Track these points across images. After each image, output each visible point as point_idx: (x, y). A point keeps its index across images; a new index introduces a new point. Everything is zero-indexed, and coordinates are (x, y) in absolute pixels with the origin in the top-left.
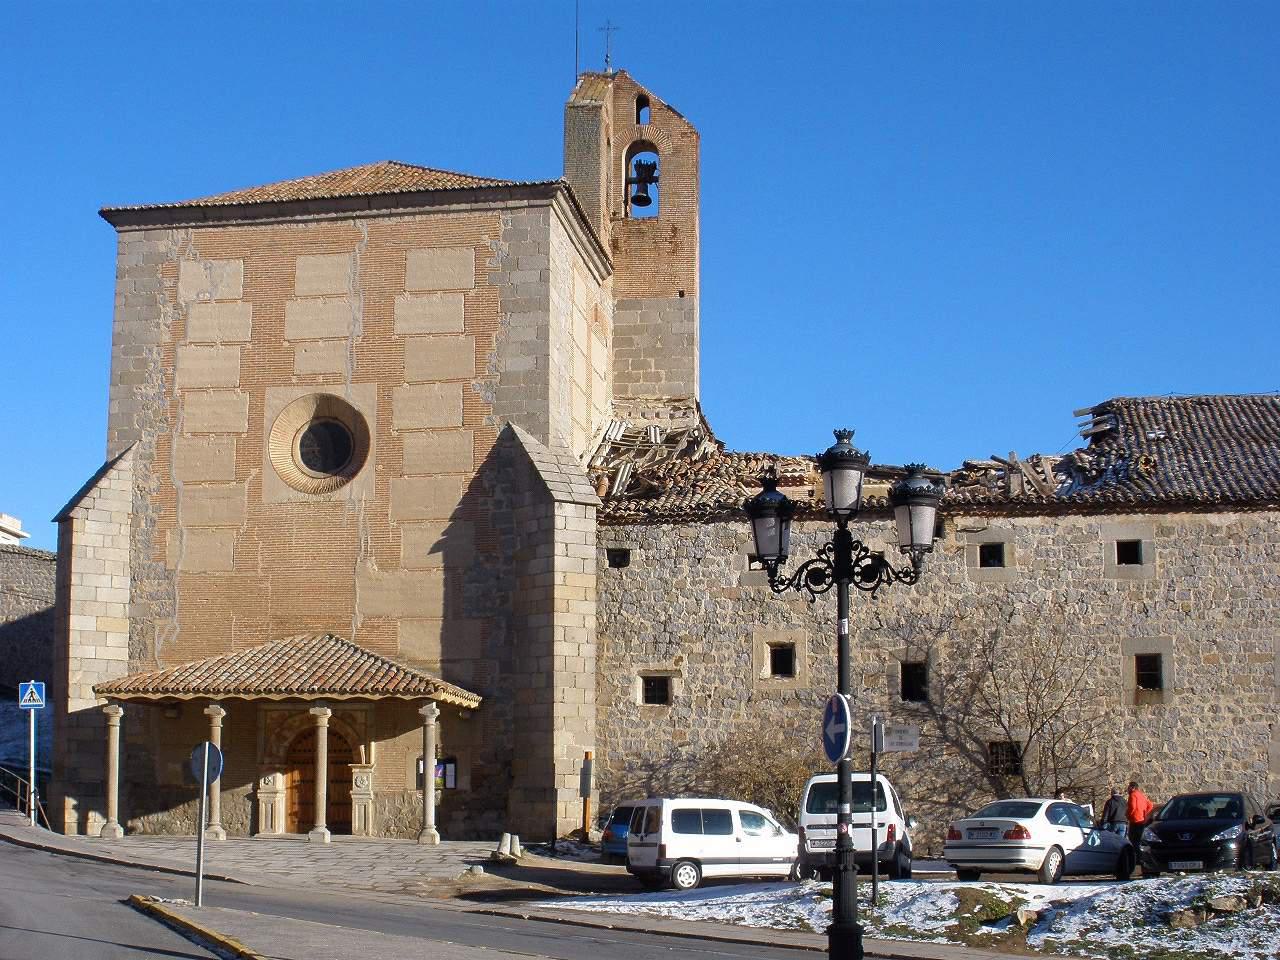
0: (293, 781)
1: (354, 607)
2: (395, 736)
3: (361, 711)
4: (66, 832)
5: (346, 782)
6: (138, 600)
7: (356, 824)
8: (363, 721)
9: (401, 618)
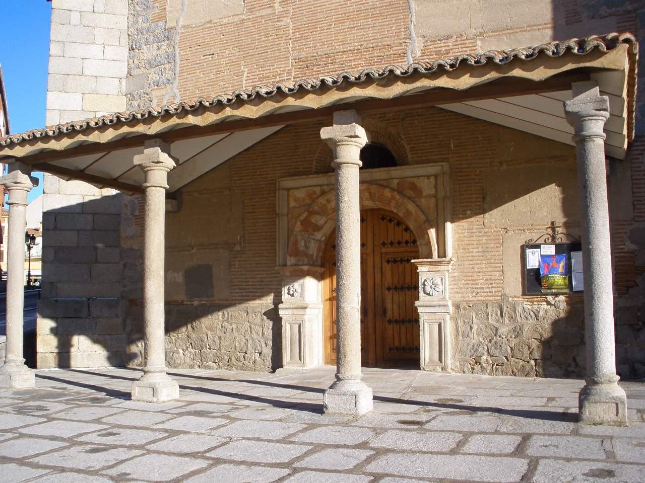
1: (409, 29)
2: (484, 211)
3: (428, 177)
4: (38, 364)
5: (409, 288)
6: (135, 72)
7: (427, 352)
8: (433, 192)
9: (481, 34)
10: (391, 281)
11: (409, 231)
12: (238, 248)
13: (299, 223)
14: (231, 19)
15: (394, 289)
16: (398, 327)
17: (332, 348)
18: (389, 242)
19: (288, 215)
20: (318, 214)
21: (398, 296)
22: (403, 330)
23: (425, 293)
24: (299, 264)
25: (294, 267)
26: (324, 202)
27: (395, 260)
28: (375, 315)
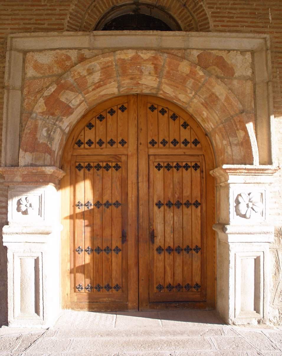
0: (76, 205)
3: (243, 52)
10: (163, 193)
11: (189, 127)
13: (41, 101)
15: (167, 204)
16: (171, 257)
17: (73, 286)
18: (161, 140)
19: (22, 89)
20: (72, 90)
21: (172, 214)
22: (179, 261)
23: (238, 213)
24: (37, 163)
25: (31, 169)
26: (85, 73)
27: (168, 164)
28: (138, 241)
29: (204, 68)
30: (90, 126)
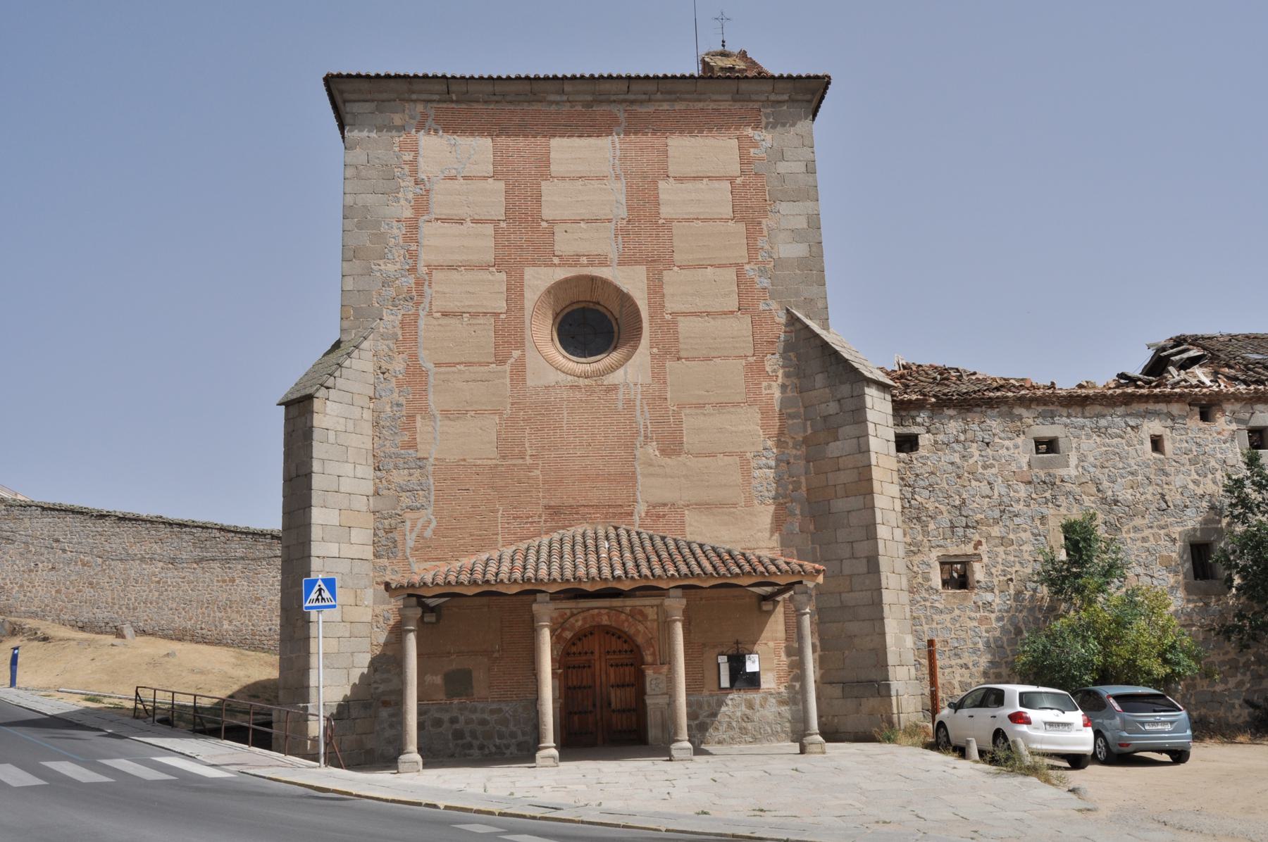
3: (652, 606)
9: (688, 506)
12: (496, 655)
14: (485, 462)
29: (632, 617)
30: (574, 644)
